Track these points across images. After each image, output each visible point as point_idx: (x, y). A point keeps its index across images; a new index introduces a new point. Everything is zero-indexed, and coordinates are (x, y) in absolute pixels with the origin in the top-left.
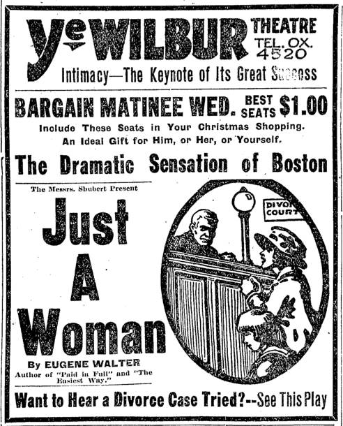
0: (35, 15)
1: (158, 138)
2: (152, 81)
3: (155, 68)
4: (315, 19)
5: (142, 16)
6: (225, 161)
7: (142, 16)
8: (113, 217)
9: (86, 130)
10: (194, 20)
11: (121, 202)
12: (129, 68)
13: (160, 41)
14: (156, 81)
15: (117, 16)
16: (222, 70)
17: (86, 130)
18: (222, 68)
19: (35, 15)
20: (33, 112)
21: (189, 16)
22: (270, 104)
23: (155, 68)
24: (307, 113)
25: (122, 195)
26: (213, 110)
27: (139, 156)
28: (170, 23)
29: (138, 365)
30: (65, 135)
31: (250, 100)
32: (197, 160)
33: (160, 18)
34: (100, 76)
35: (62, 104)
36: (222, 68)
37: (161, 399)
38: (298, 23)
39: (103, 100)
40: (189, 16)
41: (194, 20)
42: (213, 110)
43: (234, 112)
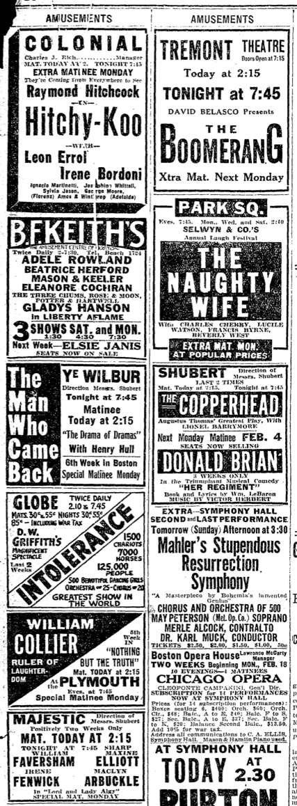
1: (132, 685)
2: (106, 133)
3: (114, 109)
5: (101, 369)
6: (50, 156)
8: (239, 793)
10: (219, 790)
11: (76, 85)
14: (115, 133)
16: (51, 115)
18: (51, 109)
22: (221, 780)
23: (114, 109)
25: (76, 83)
26: (63, 159)
27: (99, 76)
28: (113, 372)
29: (85, 407)
31: (117, 376)
32: (48, 115)
34: (63, 124)
36: (51, 109)
37: (49, 157)
41: (219, 790)
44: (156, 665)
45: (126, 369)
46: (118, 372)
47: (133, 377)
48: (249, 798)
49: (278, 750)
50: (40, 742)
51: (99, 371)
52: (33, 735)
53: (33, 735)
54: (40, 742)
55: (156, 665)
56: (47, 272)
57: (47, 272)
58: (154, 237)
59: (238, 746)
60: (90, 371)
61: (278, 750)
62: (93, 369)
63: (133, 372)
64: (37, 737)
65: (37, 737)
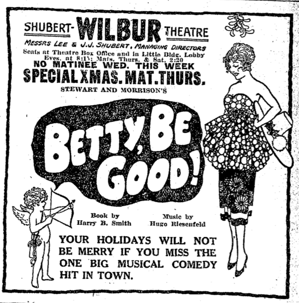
0: (18, 76)
4: (207, 29)
5: (104, 16)
7: (104, 16)
9: (181, 238)
12: (169, 27)
13: (114, 31)
15: (91, 16)
17: (181, 238)
19: (18, 76)
20: (65, 79)
21: (130, 17)
24: (48, 81)
26: (45, 78)
28: (120, 22)
30: (117, 221)
33: (114, 18)
35: (165, 72)
38: (195, 31)
39: (144, 83)
40: (130, 17)
42: (45, 78)
43: (161, 119)
44: (178, 240)
45: (139, 17)
46: (127, 22)
47: (84, 239)
48: (139, 34)
49: (137, 65)
50: (150, 82)
51: (101, 19)
52: (142, 73)
53: (142, 73)
54: (150, 82)
55: (178, 240)
56: (71, 66)
57: (71, 66)
58: (26, 9)
59: (109, 249)
60: (87, 19)
61: (137, 65)
62: (91, 16)
63: (151, 22)
64: (147, 76)
65: (147, 76)
